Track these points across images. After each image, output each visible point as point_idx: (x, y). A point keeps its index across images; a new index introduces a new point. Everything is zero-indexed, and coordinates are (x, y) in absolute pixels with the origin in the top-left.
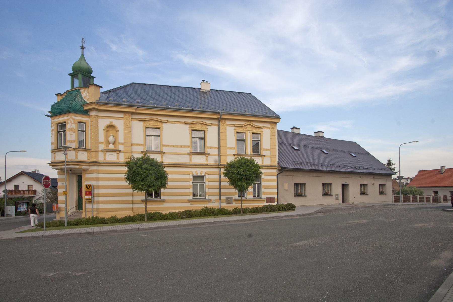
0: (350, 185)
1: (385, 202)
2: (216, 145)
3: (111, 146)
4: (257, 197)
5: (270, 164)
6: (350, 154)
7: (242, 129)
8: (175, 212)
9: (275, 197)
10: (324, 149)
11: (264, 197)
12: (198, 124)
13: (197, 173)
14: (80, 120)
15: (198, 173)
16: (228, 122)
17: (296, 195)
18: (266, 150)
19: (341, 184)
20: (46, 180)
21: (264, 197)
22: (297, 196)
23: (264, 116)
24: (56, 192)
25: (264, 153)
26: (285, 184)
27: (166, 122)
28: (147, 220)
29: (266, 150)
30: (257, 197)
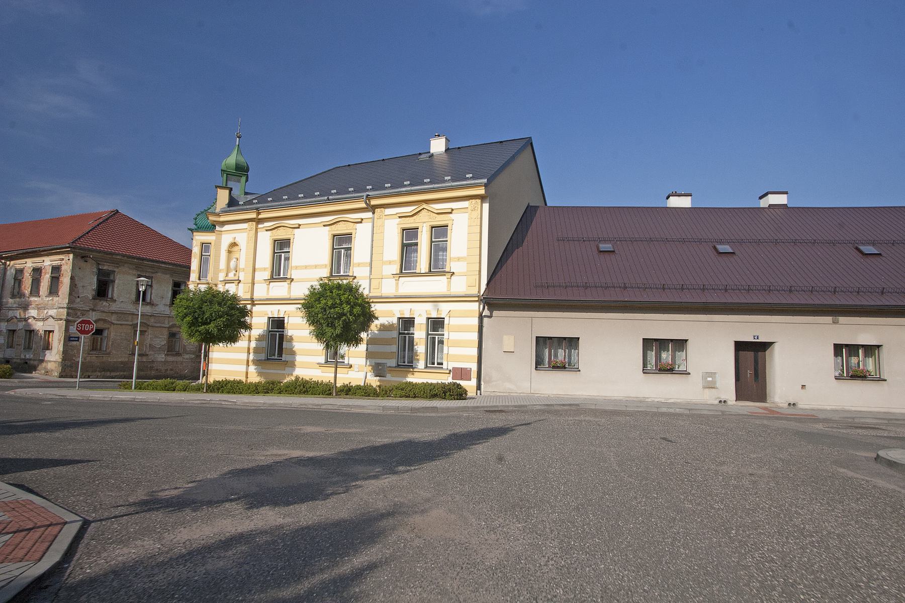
0: (777, 348)
1: (190, 402)
2: (369, 261)
3: (231, 276)
4: (437, 365)
5: (465, 290)
6: (857, 249)
7: (412, 221)
8: (436, 382)
9: (474, 367)
10: (721, 242)
11: (448, 365)
12: (340, 223)
13: (404, 314)
14: (204, 240)
15: (432, 313)
16: (389, 211)
17: (549, 367)
18: (459, 259)
19: (733, 343)
20: (83, 325)
21: (448, 365)
22: (551, 369)
23: (224, 187)
24: (750, 345)
25: (452, 266)
26: (505, 337)
27: (299, 227)
28: (207, 392)
29: (459, 259)
30: (437, 365)
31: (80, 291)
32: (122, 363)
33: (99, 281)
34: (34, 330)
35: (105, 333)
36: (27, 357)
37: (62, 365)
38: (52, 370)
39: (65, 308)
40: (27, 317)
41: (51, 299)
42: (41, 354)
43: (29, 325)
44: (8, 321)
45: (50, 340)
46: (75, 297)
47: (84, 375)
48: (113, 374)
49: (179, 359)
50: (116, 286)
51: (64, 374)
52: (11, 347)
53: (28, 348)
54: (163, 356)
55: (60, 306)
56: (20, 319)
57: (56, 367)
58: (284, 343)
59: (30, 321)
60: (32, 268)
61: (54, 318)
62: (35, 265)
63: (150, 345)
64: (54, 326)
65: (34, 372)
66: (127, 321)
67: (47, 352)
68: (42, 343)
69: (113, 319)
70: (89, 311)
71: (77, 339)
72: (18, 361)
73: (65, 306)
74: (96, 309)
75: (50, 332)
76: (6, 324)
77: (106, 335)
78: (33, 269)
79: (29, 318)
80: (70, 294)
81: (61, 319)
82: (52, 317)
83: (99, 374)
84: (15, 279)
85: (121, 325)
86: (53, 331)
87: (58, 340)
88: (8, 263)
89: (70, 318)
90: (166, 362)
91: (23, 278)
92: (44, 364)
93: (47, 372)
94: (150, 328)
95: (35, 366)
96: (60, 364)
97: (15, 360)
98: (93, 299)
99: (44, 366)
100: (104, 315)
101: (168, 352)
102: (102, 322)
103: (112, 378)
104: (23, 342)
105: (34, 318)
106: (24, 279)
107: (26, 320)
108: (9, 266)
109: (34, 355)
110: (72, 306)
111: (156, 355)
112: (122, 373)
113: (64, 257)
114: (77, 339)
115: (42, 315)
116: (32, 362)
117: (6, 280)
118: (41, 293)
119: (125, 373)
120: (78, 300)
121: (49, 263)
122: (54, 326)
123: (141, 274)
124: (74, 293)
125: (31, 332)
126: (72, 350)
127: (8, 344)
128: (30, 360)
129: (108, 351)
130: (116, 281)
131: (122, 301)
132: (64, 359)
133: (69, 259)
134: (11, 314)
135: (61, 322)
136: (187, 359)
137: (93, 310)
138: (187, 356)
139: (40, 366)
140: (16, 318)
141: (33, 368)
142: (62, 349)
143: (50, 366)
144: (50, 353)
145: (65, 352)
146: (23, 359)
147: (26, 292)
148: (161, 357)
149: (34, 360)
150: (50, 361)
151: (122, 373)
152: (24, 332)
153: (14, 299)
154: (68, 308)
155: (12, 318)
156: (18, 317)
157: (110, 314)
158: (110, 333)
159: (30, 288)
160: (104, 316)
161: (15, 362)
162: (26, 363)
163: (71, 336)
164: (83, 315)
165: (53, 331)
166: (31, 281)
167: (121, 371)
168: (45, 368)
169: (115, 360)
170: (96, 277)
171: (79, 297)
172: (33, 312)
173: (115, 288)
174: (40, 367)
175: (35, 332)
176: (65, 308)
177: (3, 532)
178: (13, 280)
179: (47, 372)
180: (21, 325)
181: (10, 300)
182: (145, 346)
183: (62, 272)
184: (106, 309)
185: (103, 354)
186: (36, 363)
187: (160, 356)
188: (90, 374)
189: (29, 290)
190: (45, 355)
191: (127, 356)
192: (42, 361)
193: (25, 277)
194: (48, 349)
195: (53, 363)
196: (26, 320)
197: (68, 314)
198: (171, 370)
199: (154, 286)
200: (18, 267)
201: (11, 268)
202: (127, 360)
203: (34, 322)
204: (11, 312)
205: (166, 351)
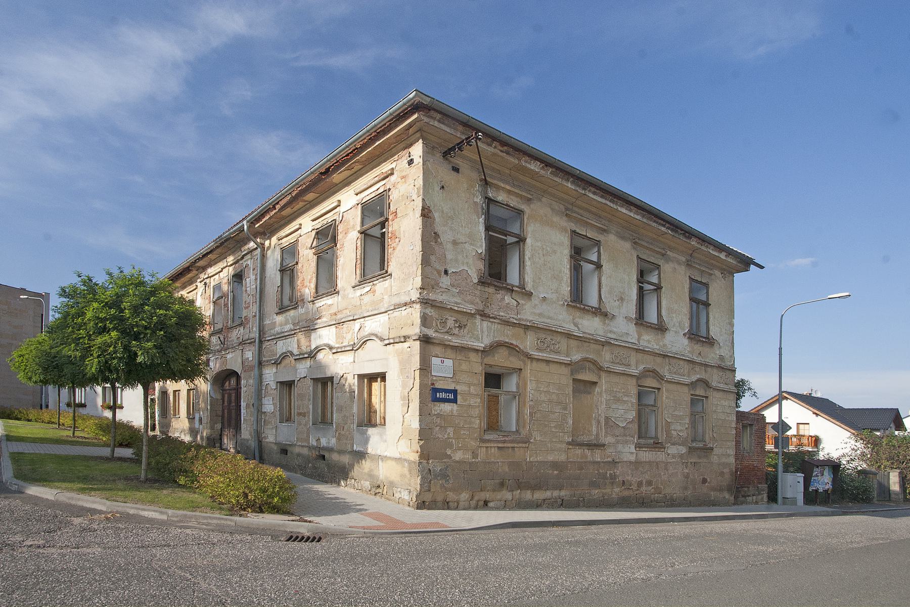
31: (450, 256)
32: (555, 465)
33: (490, 240)
34: (331, 379)
35: (511, 384)
36: (324, 442)
37: (421, 471)
38: (392, 484)
39: (413, 302)
40: (313, 347)
41: (367, 289)
42: (357, 436)
43: (320, 366)
44: (277, 363)
45: (375, 400)
46: (439, 272)
47: (476, 498)
48: (539, 495)
49: (660, 456)
50: (528, 254)
51: (428, 497)
52: (289, 420)
53: (323, 421)
54: (633, 448)
55: (396, 300)
56: (299, 355)
57: (402, 476)
58: (800, 431)
59: (320, 356)
60: (314, 233)
61: (382, 340)
62: (318, 224)
63: (607, 419)
64: (386, 359)
65: (342, 483)
66: (558, 352)
67: (371, 431)
68: (355, 410)
69: (528, 343)
70: (472, 315)
71: (451, 396)
72: (305, 451)
73: (415, 295)
74: (487, 311)
75: (372, 378)
76: (274, 370)
77: (514, 389)
78: (317, 233)
79: (318, 350)
80: (425, 262)
81: (406, 338)
82: (376, 336)
83: (508, 496)
84: (282, 271)
85: (548, 362)
86: (382, 377)
87: (403, 398)
88: (267, 243)
89: (431, 333)
90: (637, 464)
91: (297, 263)
92: (366, 465)
93: (379, 487)
94: (603, 375)
95: (344, 468)
96: (416, 468)
97: (297, 450)
98: (482, 282)
99: (366, 470)
100: (509, 331)
101: (639, 438)
102: (503, 352)
103: (176, 410)
104: (311, 407)
105: (331, 348)
106: (300, 265)
107: (312, 355)
108: (269, 248)
109: (339, 439)
110: (432, 296)
111: (620, 447)
112: (556, 493)
113: (393, 166)
114: (451, 396)
115: (349, 336)
116: (335, 457)
117: (267, 279)
118: (340, 284)
119: (563, 493)
120: (445, 281)
121: (355, 200)
122: (386, 359)
123: (578, 231)
124: (433, 258)
125: (325, 383)
126: (443, 428)
127: (281, 414)
128: (330, 450)
129: (524, 432)
130: (529, 241)
131: (544, 298)
132: (425, 455)
133: (411, 162)
134: (281, 347)
135: (406, 345)
136: (674, 456)
137: (484, 315)
138: (673, 450)
139: (356, 467)
140: (292, 354)
141: (339, 474)
142: (416, 425)
143: (386, 471)
144: (381, 435)
145: (425, 434)
146: (315, 448)
147: (307, 291)
148: (628, 452)
149: (340, 452)
150: (384, 458)
151: (556, 493)
152: (310, 383)
153: (284, 315)
154: (425, 302)
155: (284, 356)
156: (296, 352)
157: (521, 331)
158: (525, 384)
159: (314, 280)
160: (508, 335)
161: (299, 455)
162: (323, 457)
163: (438, 386)
164: (460, 327)
165: (382, 377)
166: (314, 264)
167: (555, 488)
168: (371, 476)
169: (540, 458)
170: (482, 220)
171: (446, 272)
172: (325, 336)
173: (527, 258)
174: (356, 471)
175: (335, 381)
176: (413, 302)
177: (307, 202)
178: (278, 275)
179: (379, 487)
180: (303, 368)
181: (279, 319)
182: (594, 422)
183: (392, 208)
184: (512, 317)
185: (512, 442)
186: (345, 459)
187: (626, 449)
188: (486, 495)
189: (313, 285)
190: (366, 441)
191: (564, 446)
192: (361, 455)
193: (301, 260)
194: (371, 423)
195: (392, 463)
196: (312, 355)
197: (425, 321)
198: (649, 483)
199: (606, 266)
200: (285, 242)
201: (273, 251)
202: (563, 458)
203: (331, 356)
204: (280, 343)
205: (636, 436)
